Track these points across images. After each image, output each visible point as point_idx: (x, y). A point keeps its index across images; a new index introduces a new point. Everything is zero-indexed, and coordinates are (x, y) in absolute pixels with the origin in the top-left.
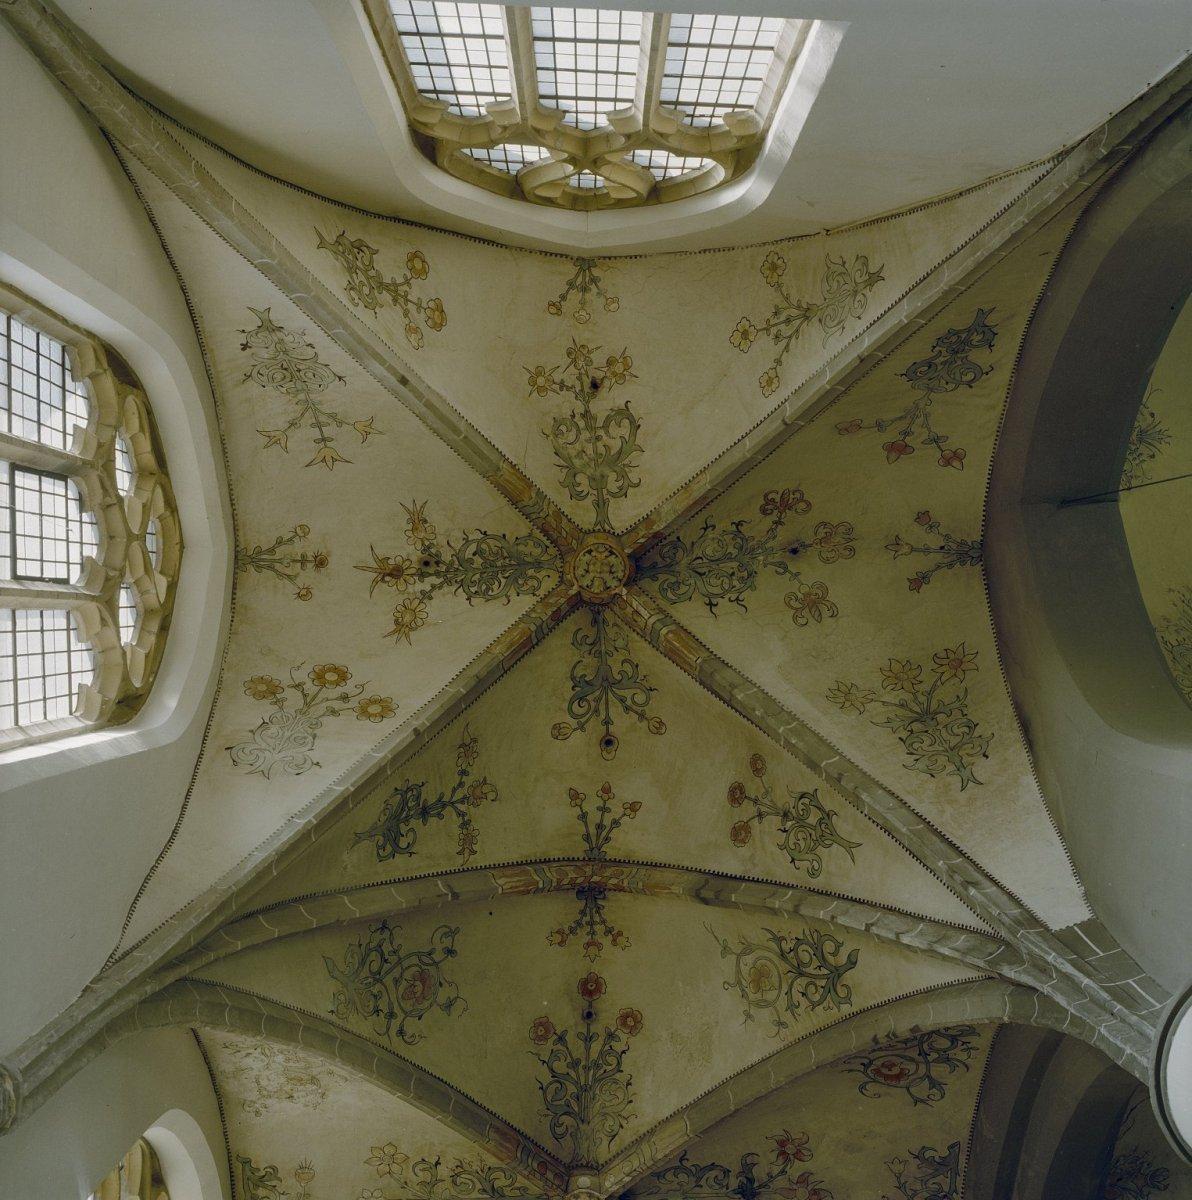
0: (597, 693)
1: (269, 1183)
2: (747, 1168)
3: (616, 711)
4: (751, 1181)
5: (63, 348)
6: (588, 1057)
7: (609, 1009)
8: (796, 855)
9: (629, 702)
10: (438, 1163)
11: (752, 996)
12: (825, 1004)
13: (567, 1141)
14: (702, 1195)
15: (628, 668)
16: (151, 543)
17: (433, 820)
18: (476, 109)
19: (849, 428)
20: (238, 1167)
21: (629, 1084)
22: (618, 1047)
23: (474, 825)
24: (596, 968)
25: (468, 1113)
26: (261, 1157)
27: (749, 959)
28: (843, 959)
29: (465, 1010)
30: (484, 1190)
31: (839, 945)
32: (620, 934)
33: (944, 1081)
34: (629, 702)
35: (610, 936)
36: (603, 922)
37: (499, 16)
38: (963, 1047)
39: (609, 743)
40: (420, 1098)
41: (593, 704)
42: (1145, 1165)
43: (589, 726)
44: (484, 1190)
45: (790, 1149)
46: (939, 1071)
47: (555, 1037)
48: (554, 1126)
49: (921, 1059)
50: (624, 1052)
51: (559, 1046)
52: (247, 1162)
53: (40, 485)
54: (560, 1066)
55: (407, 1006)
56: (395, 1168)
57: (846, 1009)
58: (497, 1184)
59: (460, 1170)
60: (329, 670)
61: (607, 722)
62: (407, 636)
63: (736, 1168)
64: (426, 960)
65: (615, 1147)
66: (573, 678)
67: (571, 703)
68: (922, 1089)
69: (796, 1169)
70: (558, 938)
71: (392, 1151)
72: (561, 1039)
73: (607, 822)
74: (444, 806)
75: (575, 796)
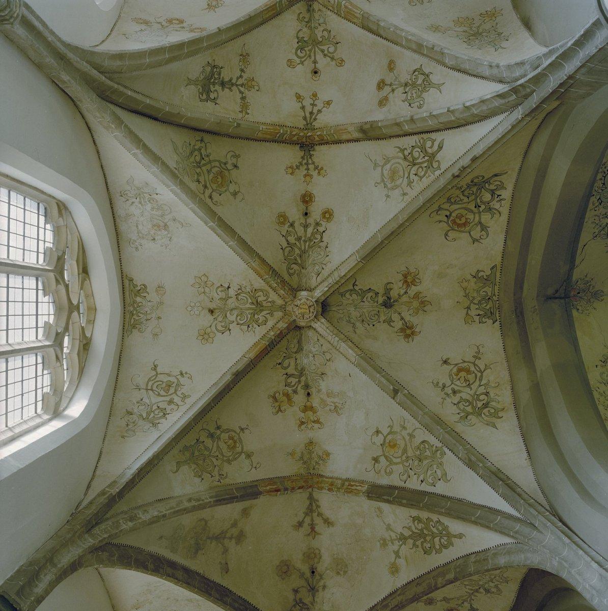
0: (310, 47)
1: (142, 294)
2: (388, 290)
3: (319, 56)
4: (389, 298)
6: (306, 236)
7: (316, 211)
8: (411, 102)
9: (326, 52)
10: (229, 287)
11: (389, 186)
12: (427, 175)
13: (295, 277)
14: (364, 307)
15: (325, 33)
17: (226, 90)
20: (127, 282)
21: (327, 247)
22: (321, 229)
23: (248, 100)
24: (309, 188)
25: (245, 247)
26: (139, 280)
27: (388, 166)
28: (436, 148)
29: (243, 199)
30: (253, 303)
31: (433, 141)
32: (322, 169)
33: (488, 225)
34: (326, 52)
35: (317, 171)
36: (313, 163)
37: (21, 357)
38: (498, 199)
39: (316, 72)
40: (220, 226)
41: (308, 52)
42: (592, 286)
43: (306, 63)
44: (253, 303)
45: (409, 279)
46: (486, 217)
47: (289, 224)
48: (289, 268)
49: (475, 210)
50: (324, 232)
51: (291, 229)
52: (131, 280)
54: (292, 239)
55: (214, 186)
56: (207, 290)
57: (438, 173)
58: (260, 299)
59: (240, 291)
60: (175, 20)
61: (315, 62)
62: (214, 10)
63: (381, 291)
64: (223, 165)
65: (319, 279)
66: (298, 38)
67: (297, 50)
68: (476, 233)
69: (413, 290)
70: (290, 171)
71: (206, 280)
72: (292, 225)
73: (315, 111)
74: (233, 85)
75: (299, 97)
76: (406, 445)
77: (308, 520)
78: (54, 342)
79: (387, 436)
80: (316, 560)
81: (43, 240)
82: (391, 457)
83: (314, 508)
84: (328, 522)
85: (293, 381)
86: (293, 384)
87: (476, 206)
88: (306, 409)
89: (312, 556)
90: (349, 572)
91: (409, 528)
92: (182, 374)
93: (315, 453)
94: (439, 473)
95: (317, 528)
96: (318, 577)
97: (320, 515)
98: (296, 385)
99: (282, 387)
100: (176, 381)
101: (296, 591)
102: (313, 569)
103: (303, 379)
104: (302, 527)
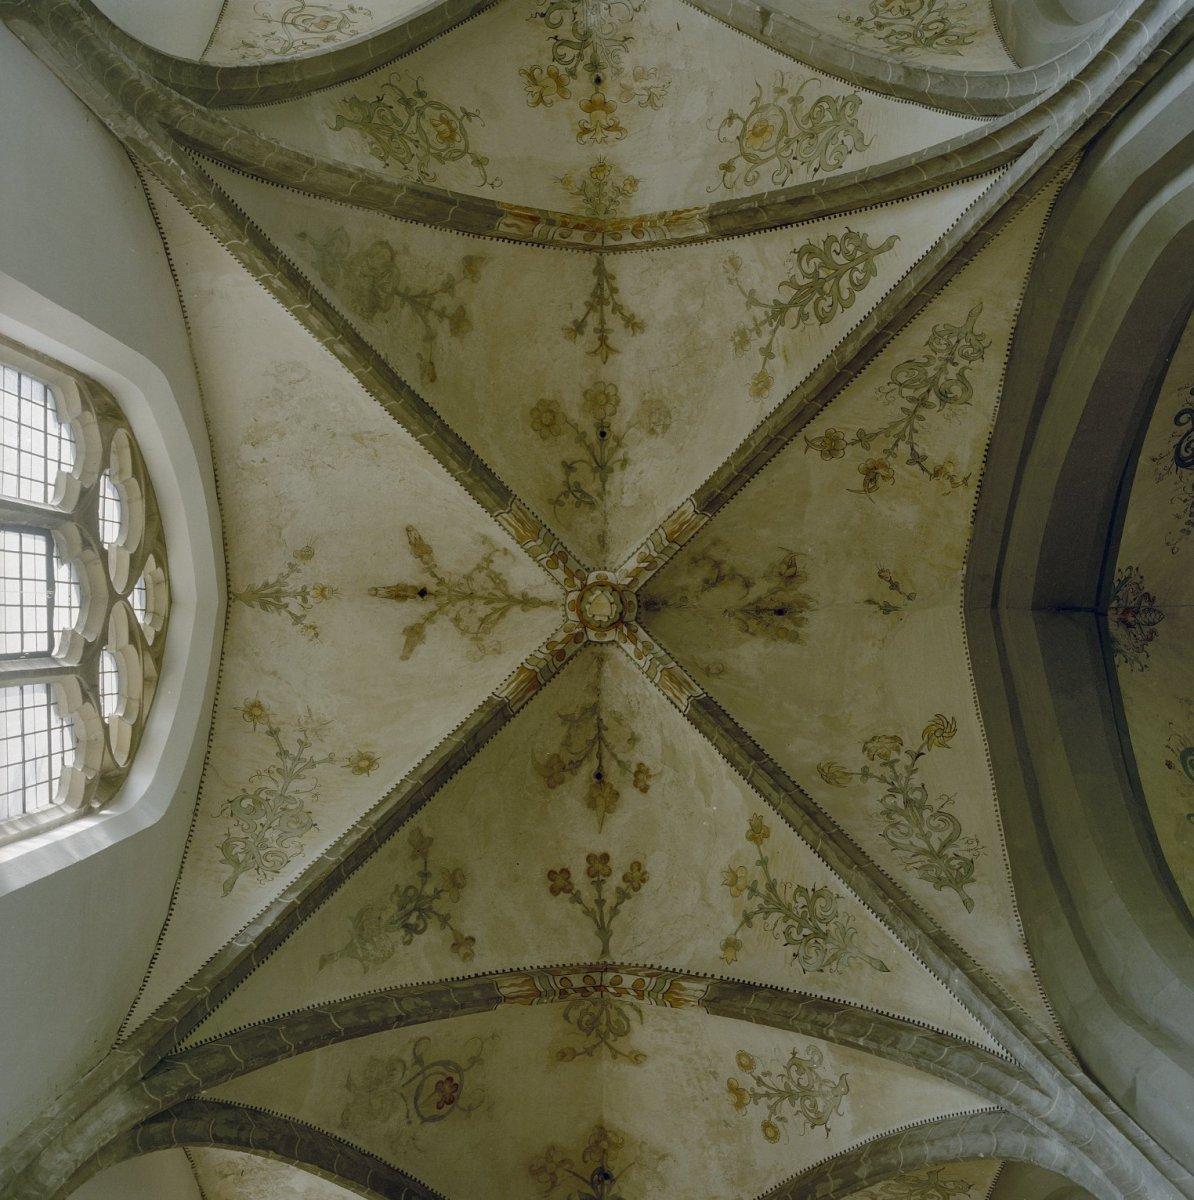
5: (46, 388)
16: (136, 599)
18: (66, 729)
19: (430, 373)
53: (19, 387)
76: (786, 122)
77: (593, 321)
78: (80, 663)
79: (748, 119)
80: (609, 409)
81: (57, 459)
82: (757, 153)
83: (607, 293)
84: (633, 324)
85: (570, 53)
86: (567, 59)
88: (591, 106)
89: (601, 398)
90: (673, 425)
91: (791, 283)
92: (352, 9)
93: (610, 184)
94: (849, 141)
95: (612, 340)
96: (612, 444)
97: (617, 308)
98: (574, 63)
99: (546, 61)
100: (340, 16)
101: (569, 467)
102: (603, 427)
103: (588, 51)
104: (582, 333)
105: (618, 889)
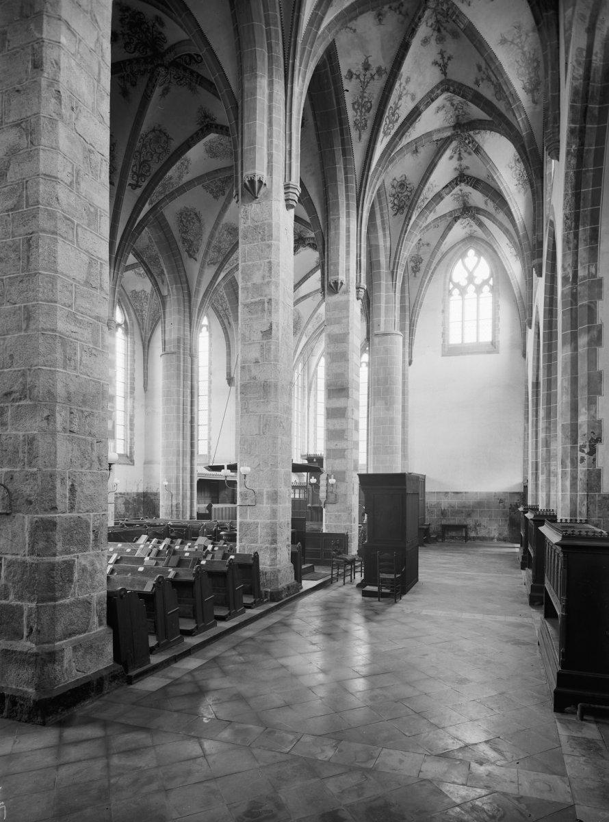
46: (394, 192)
72: (465, 151)
77: (446, 60)
84: (435, 63)
87: (398, 195)
89: (440, 40)
97: (440, 65)
105: (584, 761)
